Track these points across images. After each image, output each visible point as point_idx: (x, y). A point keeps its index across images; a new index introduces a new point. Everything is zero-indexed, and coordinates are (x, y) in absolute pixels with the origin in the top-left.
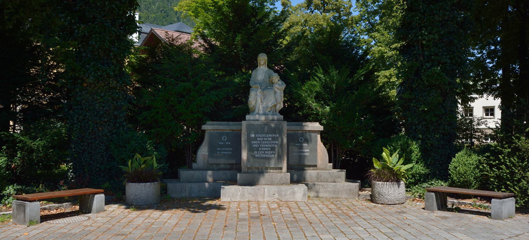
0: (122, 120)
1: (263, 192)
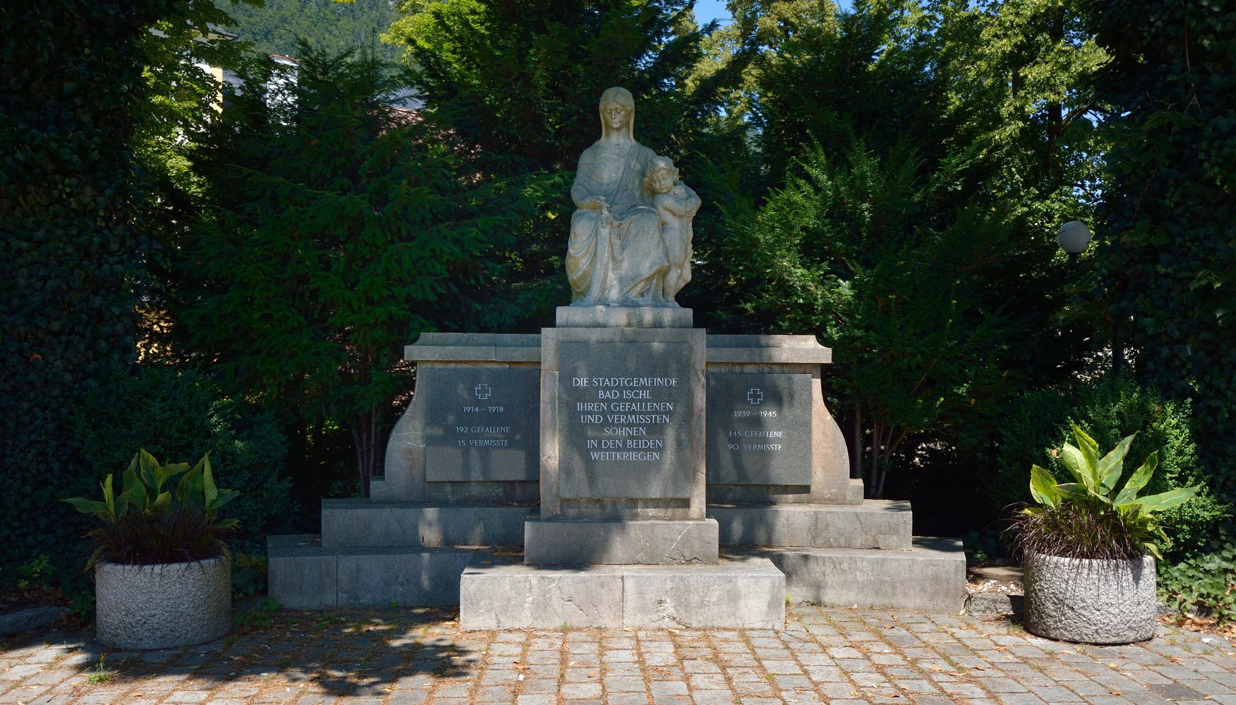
0: (119, 327)
1: (618, 595)
